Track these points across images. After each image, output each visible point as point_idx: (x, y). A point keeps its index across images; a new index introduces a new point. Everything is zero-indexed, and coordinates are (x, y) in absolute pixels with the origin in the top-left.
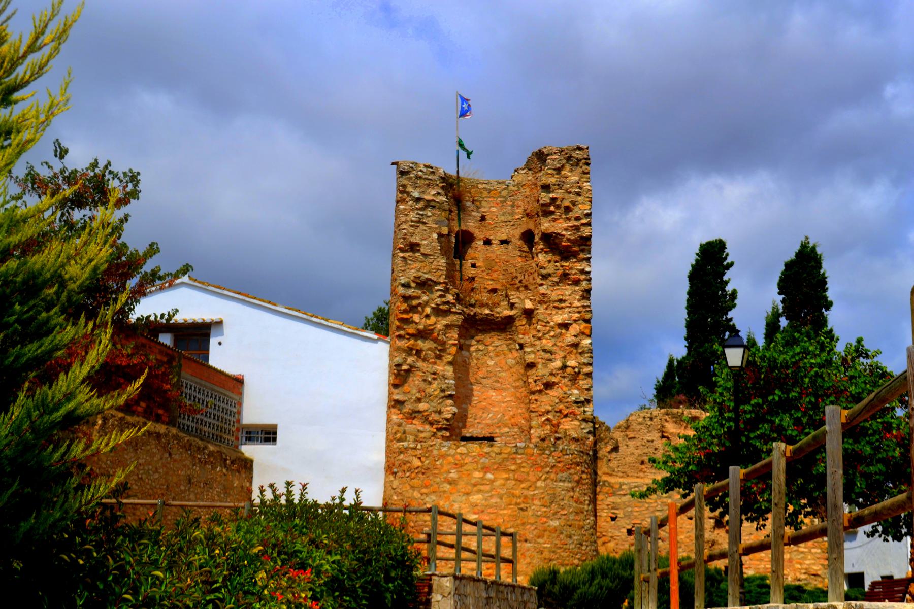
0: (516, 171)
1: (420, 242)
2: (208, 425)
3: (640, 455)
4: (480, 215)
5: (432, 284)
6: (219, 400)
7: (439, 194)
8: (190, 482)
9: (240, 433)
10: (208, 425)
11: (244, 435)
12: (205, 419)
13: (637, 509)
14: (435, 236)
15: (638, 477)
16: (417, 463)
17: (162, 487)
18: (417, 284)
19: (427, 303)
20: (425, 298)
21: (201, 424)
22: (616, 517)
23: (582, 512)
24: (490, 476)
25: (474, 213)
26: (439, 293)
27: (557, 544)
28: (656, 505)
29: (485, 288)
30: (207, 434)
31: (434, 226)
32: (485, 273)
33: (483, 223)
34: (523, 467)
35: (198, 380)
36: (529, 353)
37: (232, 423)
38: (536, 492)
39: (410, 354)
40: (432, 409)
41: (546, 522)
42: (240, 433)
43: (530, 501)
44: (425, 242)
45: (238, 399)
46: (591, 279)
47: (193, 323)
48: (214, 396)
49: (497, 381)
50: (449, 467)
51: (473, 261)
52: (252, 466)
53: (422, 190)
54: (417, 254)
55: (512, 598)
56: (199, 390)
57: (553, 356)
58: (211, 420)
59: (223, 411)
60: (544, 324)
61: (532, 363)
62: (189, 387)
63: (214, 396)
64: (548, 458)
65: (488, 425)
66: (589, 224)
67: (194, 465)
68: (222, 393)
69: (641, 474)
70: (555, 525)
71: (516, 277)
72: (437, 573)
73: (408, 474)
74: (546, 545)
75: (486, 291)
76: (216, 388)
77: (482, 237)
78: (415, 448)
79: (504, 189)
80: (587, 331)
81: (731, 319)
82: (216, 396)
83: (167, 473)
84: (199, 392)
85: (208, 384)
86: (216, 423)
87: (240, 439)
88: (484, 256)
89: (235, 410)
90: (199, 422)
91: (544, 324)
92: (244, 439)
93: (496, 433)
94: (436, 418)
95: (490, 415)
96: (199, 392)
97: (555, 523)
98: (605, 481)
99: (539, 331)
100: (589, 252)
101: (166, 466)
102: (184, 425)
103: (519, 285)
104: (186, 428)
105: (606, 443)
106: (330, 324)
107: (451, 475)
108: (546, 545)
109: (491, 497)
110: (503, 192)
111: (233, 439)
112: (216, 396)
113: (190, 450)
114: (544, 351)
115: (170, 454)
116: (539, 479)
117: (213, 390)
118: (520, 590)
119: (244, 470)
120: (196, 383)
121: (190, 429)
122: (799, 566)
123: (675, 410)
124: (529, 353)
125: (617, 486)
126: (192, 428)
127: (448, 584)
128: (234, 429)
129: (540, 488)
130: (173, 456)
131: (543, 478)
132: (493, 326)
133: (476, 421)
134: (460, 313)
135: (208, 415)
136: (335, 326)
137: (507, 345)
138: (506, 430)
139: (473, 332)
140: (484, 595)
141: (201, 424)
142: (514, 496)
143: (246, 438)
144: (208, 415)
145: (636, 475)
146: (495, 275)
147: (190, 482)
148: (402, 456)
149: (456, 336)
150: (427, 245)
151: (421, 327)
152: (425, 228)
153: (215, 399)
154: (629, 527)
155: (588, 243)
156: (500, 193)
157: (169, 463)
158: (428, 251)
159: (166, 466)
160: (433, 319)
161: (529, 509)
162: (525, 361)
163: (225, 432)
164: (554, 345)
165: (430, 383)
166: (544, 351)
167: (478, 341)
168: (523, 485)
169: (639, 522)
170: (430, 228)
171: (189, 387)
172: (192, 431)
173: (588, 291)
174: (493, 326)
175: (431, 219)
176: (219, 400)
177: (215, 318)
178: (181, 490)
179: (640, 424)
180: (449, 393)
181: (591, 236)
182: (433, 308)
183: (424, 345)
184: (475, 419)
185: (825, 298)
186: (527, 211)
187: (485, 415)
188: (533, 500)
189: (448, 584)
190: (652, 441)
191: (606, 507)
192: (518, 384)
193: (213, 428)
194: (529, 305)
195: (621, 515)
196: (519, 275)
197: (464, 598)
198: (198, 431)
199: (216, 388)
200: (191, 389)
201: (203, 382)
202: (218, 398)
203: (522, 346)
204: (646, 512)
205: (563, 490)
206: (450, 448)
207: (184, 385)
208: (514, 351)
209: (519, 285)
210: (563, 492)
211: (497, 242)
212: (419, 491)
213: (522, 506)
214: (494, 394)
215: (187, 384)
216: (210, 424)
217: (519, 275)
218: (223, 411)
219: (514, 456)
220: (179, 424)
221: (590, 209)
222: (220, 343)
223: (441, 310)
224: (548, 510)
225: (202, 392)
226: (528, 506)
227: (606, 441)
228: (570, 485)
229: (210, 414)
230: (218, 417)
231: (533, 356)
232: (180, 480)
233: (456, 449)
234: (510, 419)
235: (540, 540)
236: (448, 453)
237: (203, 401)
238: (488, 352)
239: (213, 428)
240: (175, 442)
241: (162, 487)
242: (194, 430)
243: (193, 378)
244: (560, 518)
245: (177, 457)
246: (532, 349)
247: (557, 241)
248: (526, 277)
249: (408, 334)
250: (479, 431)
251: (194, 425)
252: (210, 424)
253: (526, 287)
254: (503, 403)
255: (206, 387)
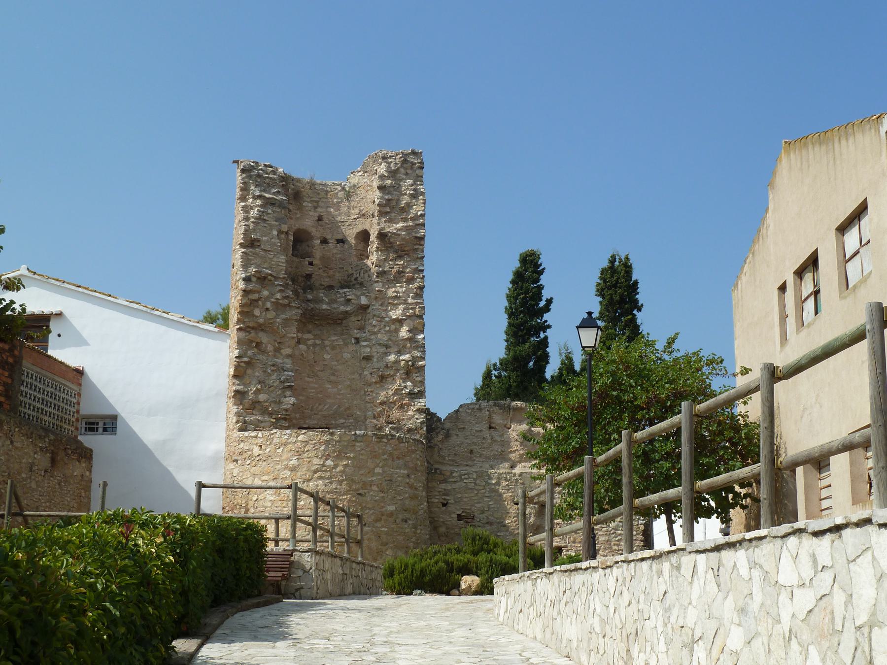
0: (352, 173)
1: (261, 238)
2: (48, 414)
3: (469, 445)
4: (317, 215)
5: (273, 279)
6: (60, 390)
7: (278, 192)
8: (31, 470)
9: (80, 423)
10: (48, 414)
11: (84, 425)
12: (46, 409)
13: (467, 495)
14: (275, 233)
15: (467, 465)
16: (256, 451)
17: (4, 474)
18: (258, 278)
19: (267, 298)
20: (266, 293)
21: (42, 413)
22: (447, 503)
23: (417, 498)
24: (329, 463)
25: (311, 213)
26: (279, 288)
27: (393, 528)
28: (484, 491)
29: (322, 285)
30: (47, 423)
31: (274, 223)
32: (321, 271)
33: (320, 222)
34: (362, 455)
35: (39, 370)
36: (365, 346)
37: (72, 413)
38: (374, 478)
39: (251, 348)
40: (271, 400)
41: (383, 507)
42: (80, 423)
43: (369, 487)
44: (265, 239)
45: (78, 390)
46: (424, 277)
47: (32, 315)
48: (54, 386)
49: (334, 375)
50: (290, 454)
51: (310, 260)
52: (91, 455)
53: (263, 188)
54: (258, 250)
55: (362, 576)
56: (40, 379)
57: (389, 350)
58: (52, 410)
59: (63, 402)
60: (379, 319)
61: (367, 356)
62: (30, 376)
63: (54, 386)
64: (385, 446)
65: (325, 416)
66: (423, 225)
67: (35, 453)
68: (62, 384)
69: (470, 463)
70: (392, 509)
71: (352, 275)
72: (298, 548)
73: (248, 462)
74: (383, 529)
75: (323, 287)
76: (56, 378)
77: (319, 236)
78: (256, 437)
79: (340, 191)
80: (420, 327)
81: (546, 321)
82: (56, 386)
83: (8, 460)
84: (40, 382)
85: (49, 374)
86: (56, 412)
87: (80, 429)
88: (321, 255)
89: (74, 400)
90: (40, 411)
91: (379, 319)
92: (83, 429)
93: (332, 424)
94: (275, 409)
95: (326, 407)
96: (40, 382)
97: (391, 508)
98: (436, 469)
99: (375, 326)
100: (423, 251)
101: (7, 454)
102: (24, 414)
103: (355, 282)
104: (27, 417)
105: (437, 433)
106: (171, 317)
107: (292, 462)
108: (383, 529)
109: (331, 483)
110: (339, 193)
111: (73, 429)
112: (56, 386)
113: (31, 438)
114: (380, 344)
115: (12, 442)
116: (377, 466)
117: (53, 380)
118: (369, 568)
119: (84, 460)
120: (37, 372)
121: (31, 418)
122: (616, 548)
123: (502, 402)
124: (365, 346)
125: (448, 474)
126: (33, 417)
127: (309, 560)
128: (73, 419)
129: (379, 474)
130: (15, 443)
131: (380, 465)
132: (330, 321)
133: (313, 412)
134: (298, 308)
135: (49, 404)
136: (176, 319)
137: (343, 340)
138: (342, 421)
139: (310, 327)
140: (340, 571)
141: (42, 413)
142: (353, 481)
143: (86, 428)
144: (49, 404)
145: (465, 463)
146: (331, 273)
147: (31, 470)
148: (242, 445)
149: (295, 330)
150: (267, 241)
151: (261, 321)
152: (265, 225)
153: (56, 389)
154: (459, 513)
155: (422, 243)
156: (337, 193)
157: (10, 451)
158: (268, 247)
159: (7, 454)
160: (271, 314)
161: (367, 494)
162: (361, 354)
163: (65, 422)
164: (390, 340)
165: (270, 375)
166: (380, 344)
167: (315, 336)
168: (362, 472)
169: (469, 507)
170: (270, 225)
171: (30, 376)
172: (33, 420)
173: (421, 288)
174: (330, 321)
175: (271, 216)
176: (60, 390)
177: (55, 309)
178: (23, 478)
179: (470, 415)
180: (289, 384)
181: (425, 236)
182: (272, 302)
183: (264, 338)
184: (311, 411)
185: (637, 301)
186: (363, 212)
187: (320, 407)
188: (371, 486)
189: (309, 560)
190: (481, 431)
191: (438, 494)
192: (353, 377)
193: (54, 418)
194: (364, 301)
195: (452, 501)
196: (355, 273)
197: (324, 573)
198: (39, 420)
199: (56, 378)
200: (32, 378)
201: (44, 372)
202: (58, 388)
203: (357, 341)
204: (476, 498)
205: (399, 477)
206: (291, 436)
207: (26, 374)
208: (350, 346)
209: (355, 282)
210: (399, 479)
211: (333, 241)
212: (260, 479)
213: (360, 492)
214: (330, 386)
215: (28, 373)
216: (50, 413)
217: (355, 273)
218: (63, 402)
219: (354, 443)
220: (20, 413)
221: (423, 211)
222: (59, 335)
223: (281, 304)
224: (385, 495)
225: (42, 382)
226: (366, 491)
227: (438, 431)
228: (406, 472)
229: (51, 404)
230: (59, 407)
231: (368, 350)
232: (21, 468)
233: (297, 437)
234: (345, 410)
235: (378, 525)
236: (289, 441)
237: (44, 391)
238: (325, 346)
239: (54, 418)
240: (17, 429)
241: (4, 474)
242: (35, 419)
243: (34, 368)
244: (396, 504)
245: (18, 445)
246: (368, 343)
247: (392, 240)
248: (362, 274)
249: (249, 327)
250: (316, 422)
251: (35, 414)
252: (50, 413)
253: (362, 284)
254: (339, 395)
255: (47, 377)
